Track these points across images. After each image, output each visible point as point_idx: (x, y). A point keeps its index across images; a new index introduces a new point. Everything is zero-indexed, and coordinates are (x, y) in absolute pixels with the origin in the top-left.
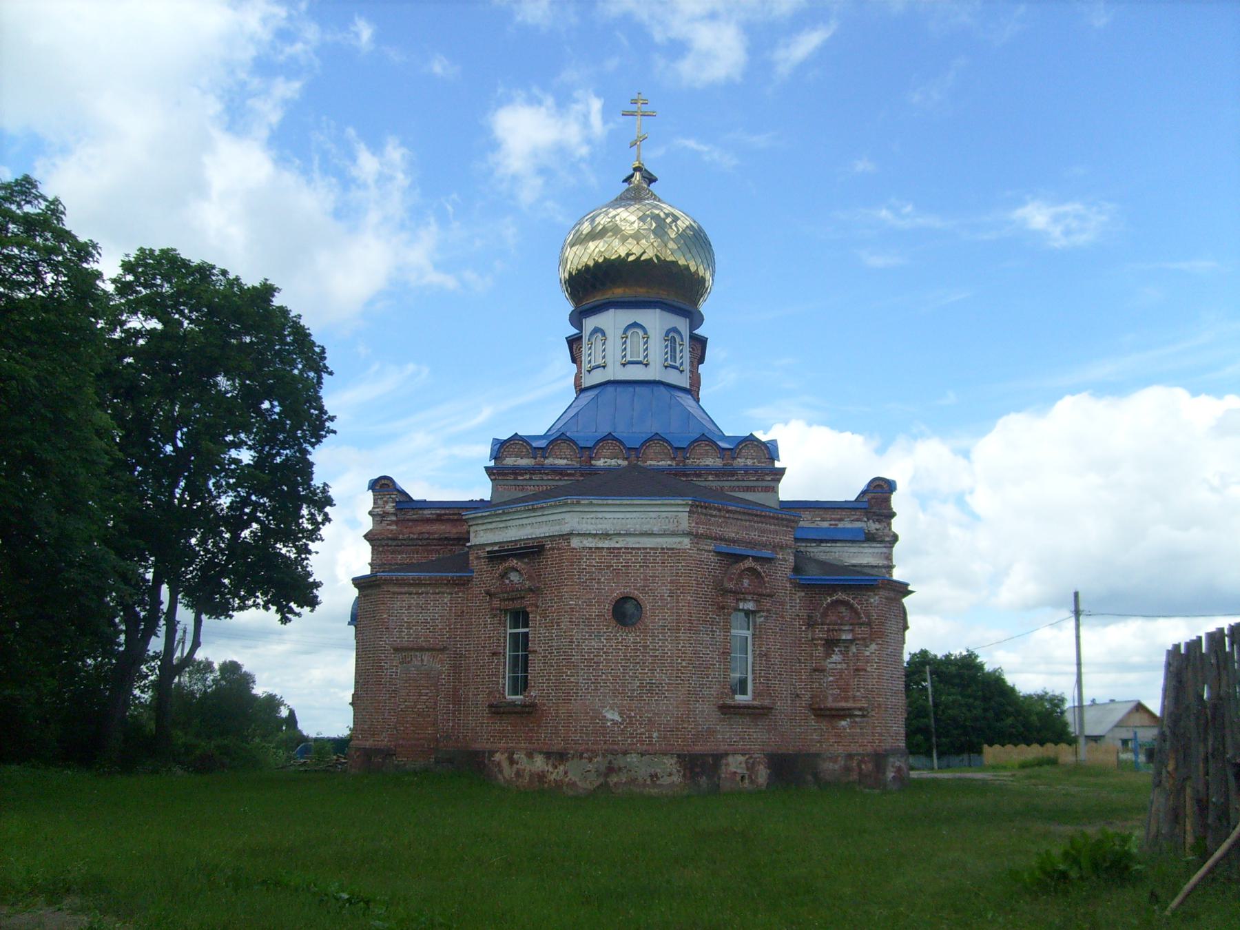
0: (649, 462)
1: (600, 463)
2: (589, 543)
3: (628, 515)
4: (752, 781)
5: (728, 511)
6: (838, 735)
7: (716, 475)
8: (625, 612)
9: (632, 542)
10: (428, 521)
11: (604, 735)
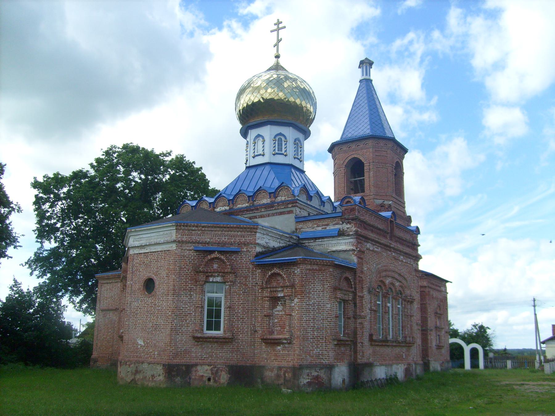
0: (238, 206)
1: (218, 210)
3: (152, 235)
4: (215, 381)
5: (203, 227)
6: (276, 355)
7: (265, 208)
8: (149, 285)
9: (153, 249)
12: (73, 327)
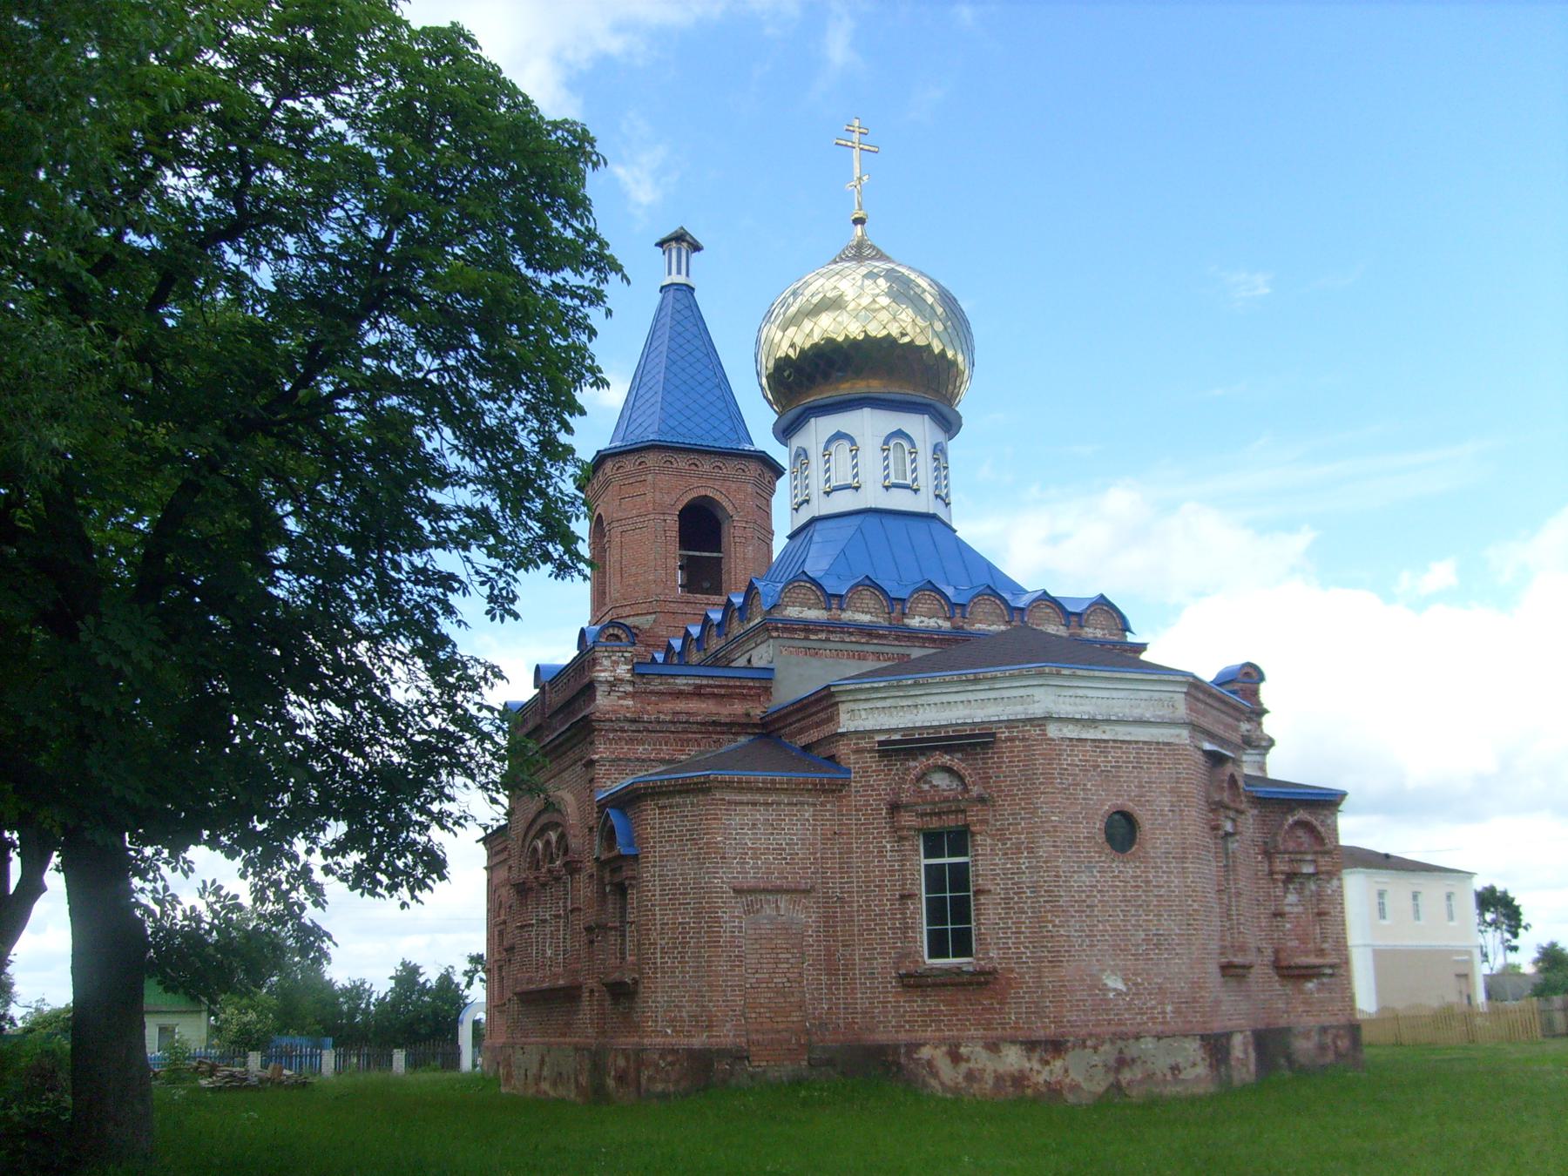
0: (978, 626)
1: (915, 622)
2: (1071, 732)
3: (1115, 694)
6: (1305, 1002)
8: (1122, 831)
9: (1122, 733)
10: (679, 695)
11: (1107, 1011)
12: (9, 970)
